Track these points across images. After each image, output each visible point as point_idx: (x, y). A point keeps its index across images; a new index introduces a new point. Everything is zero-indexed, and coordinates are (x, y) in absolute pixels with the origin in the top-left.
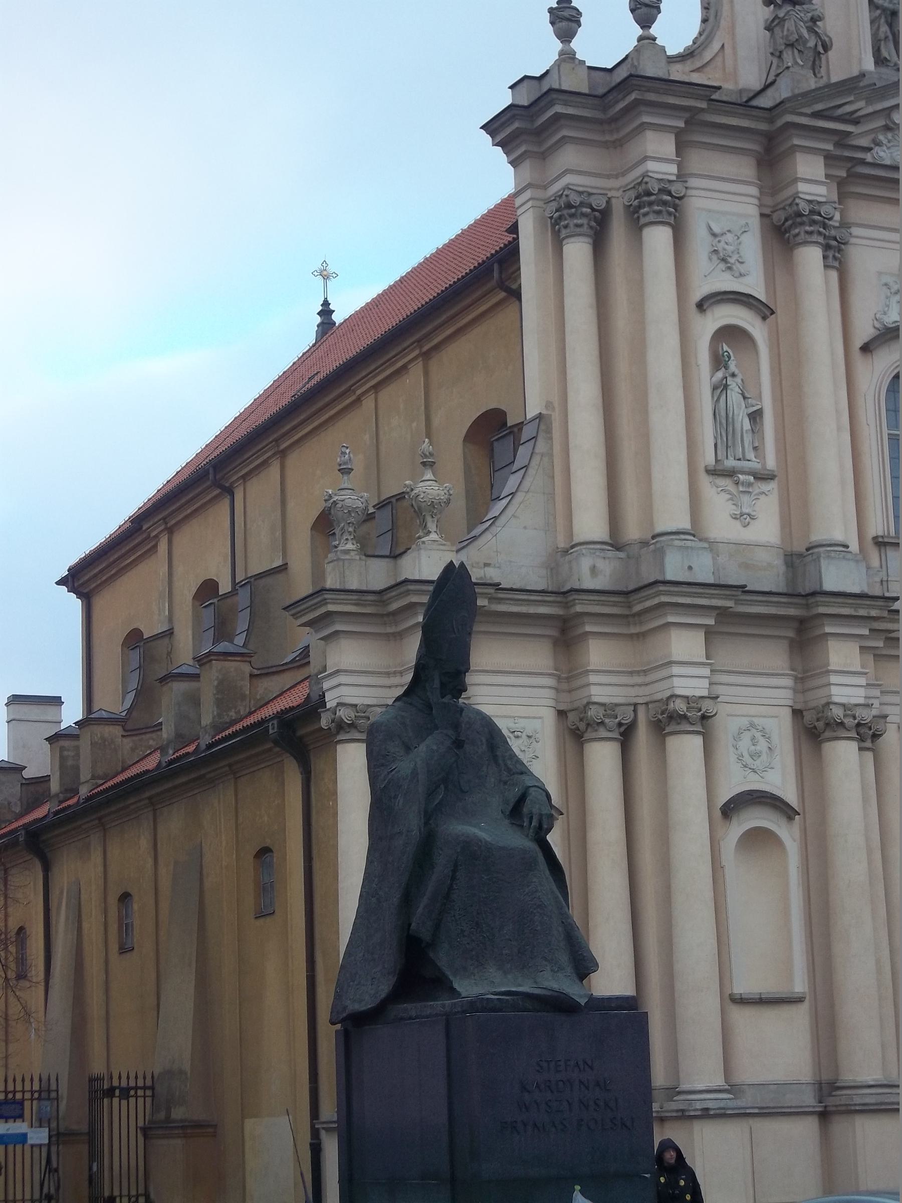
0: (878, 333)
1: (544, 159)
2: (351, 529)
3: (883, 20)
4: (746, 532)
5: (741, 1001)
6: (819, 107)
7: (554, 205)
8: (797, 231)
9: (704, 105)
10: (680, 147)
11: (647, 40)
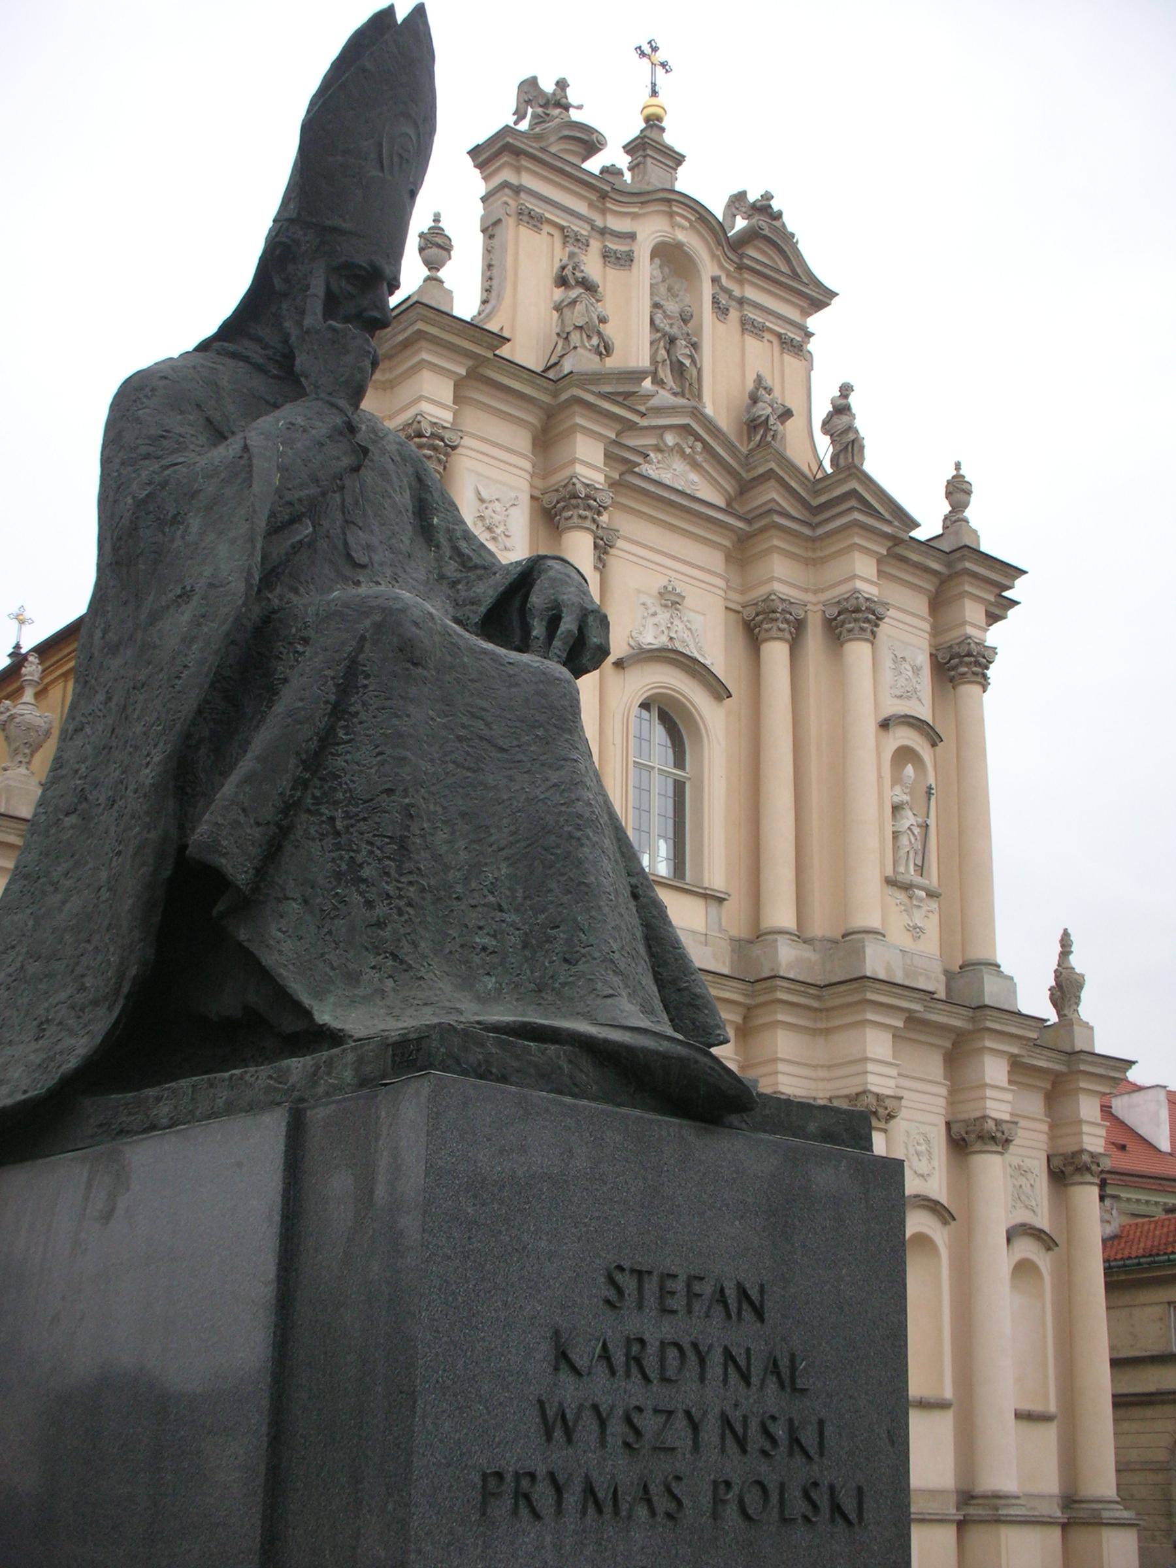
0: (632, 651)
2: (27, 751)
3: (662, 344)
6: (607, 389)
8: (570, 513)
9: (490, 355)
10: (457, 399)
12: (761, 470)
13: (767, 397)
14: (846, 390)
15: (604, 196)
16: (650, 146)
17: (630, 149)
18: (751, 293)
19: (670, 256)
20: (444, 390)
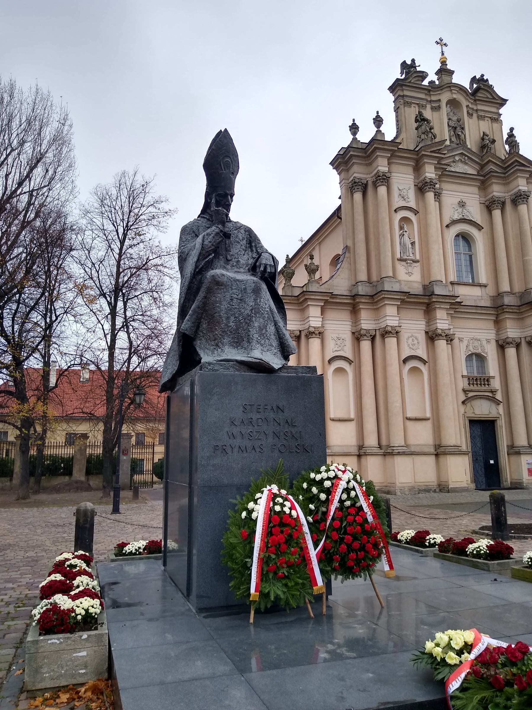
1: (348, 171)
4: (410, 278)
5: (409, 419)
6: (432, 149)
7: (351, 184)
9: (396, 149)
11: (379, 132)
12: (486, 161)
13: (487, 138)
14: (512, 129)
15: (429, 91)
16: (444, 71)
17: (437, 73)
18: (480, 107)
19: (453, 103)
20: (385, 162)
